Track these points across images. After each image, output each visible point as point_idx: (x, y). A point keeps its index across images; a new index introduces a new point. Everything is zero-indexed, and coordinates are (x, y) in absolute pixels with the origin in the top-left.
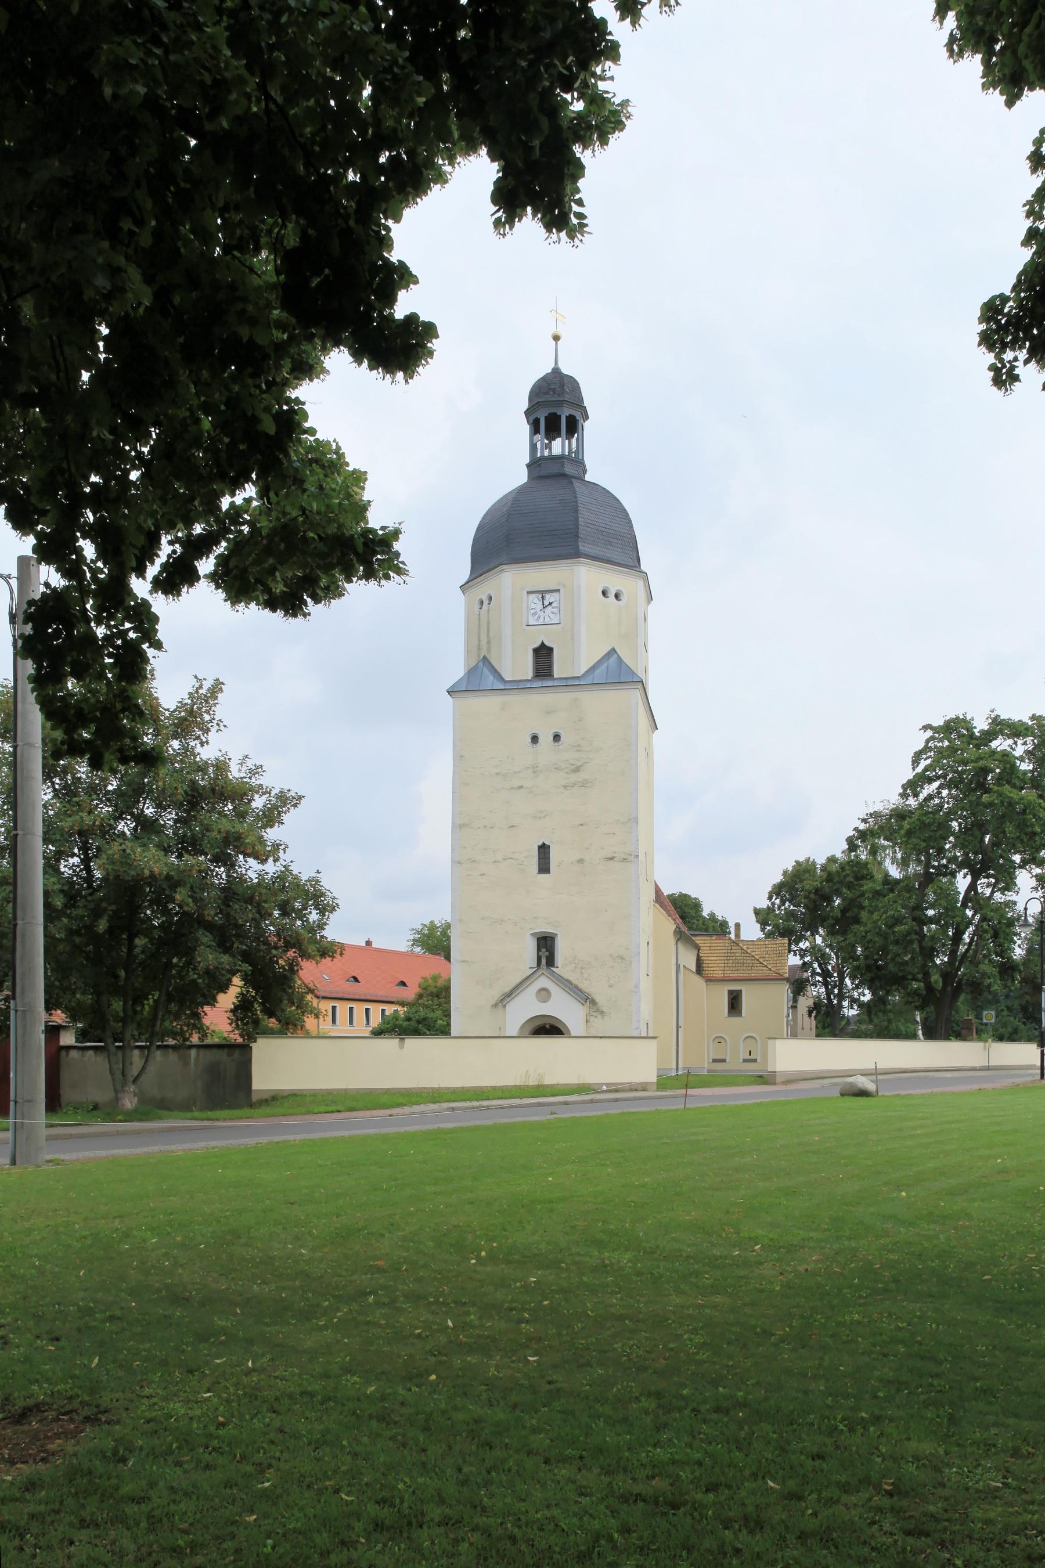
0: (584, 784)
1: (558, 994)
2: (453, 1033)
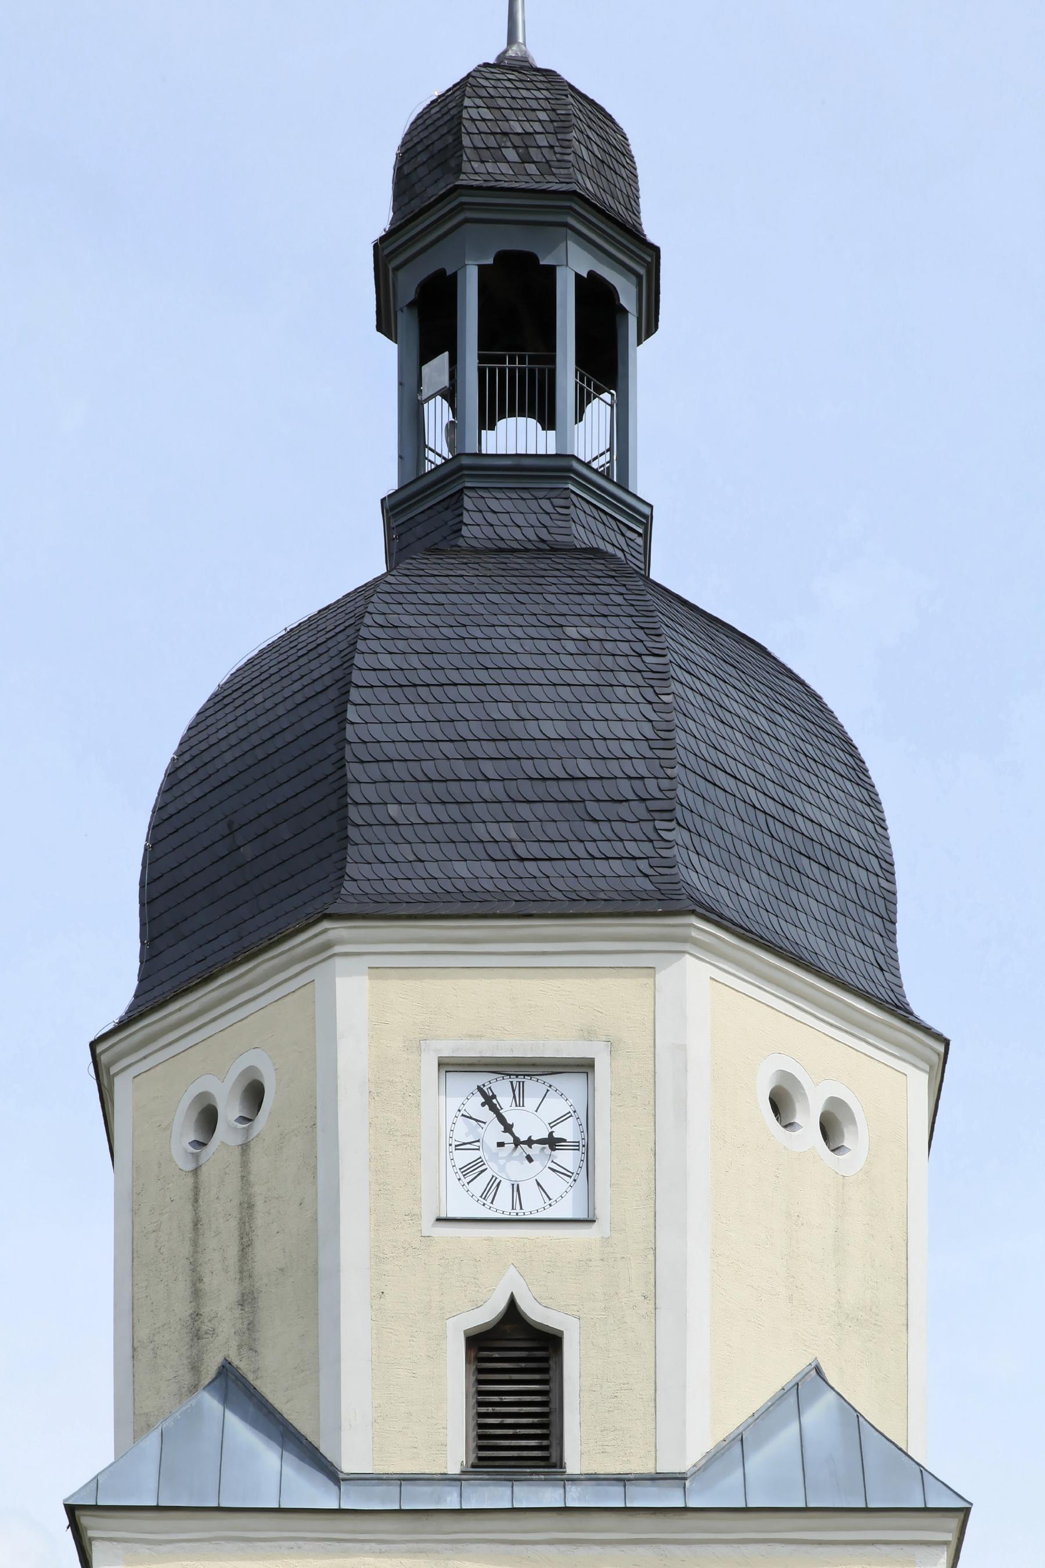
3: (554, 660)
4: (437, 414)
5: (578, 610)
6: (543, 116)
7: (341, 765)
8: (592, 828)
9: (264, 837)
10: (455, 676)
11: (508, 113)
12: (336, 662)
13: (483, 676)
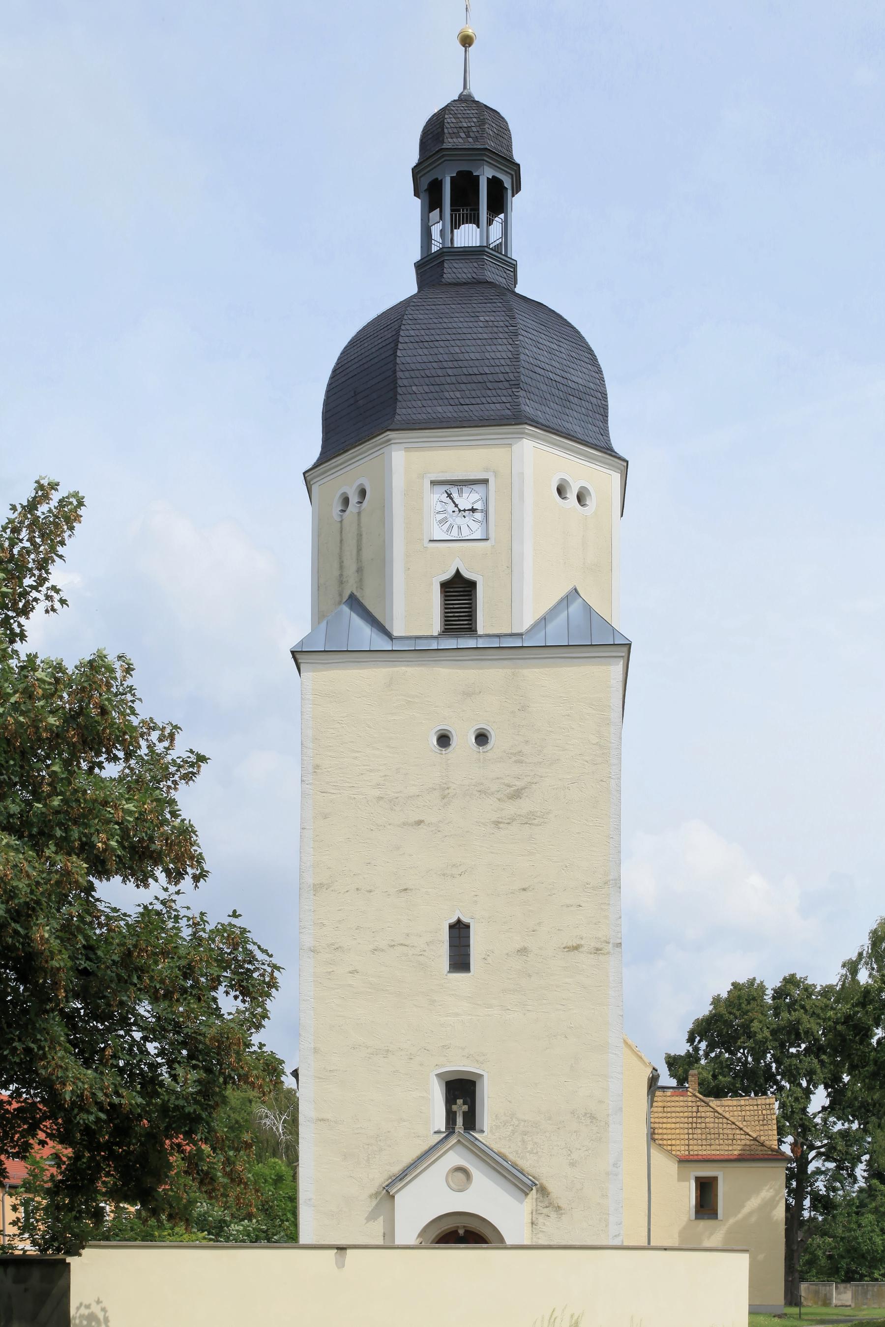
0: (529, 820)
1: (481, 1179)
2: (303, 1239)
3: (475, 330)
4: (436, 230)
5: (484, 310)
6: (475, 120)
7: (395, 372)
8: (489, 392)
9: (369, 396)
10: (438, 338)
11: (462, 120)
12: (394, 333)
13: (448, 337)
